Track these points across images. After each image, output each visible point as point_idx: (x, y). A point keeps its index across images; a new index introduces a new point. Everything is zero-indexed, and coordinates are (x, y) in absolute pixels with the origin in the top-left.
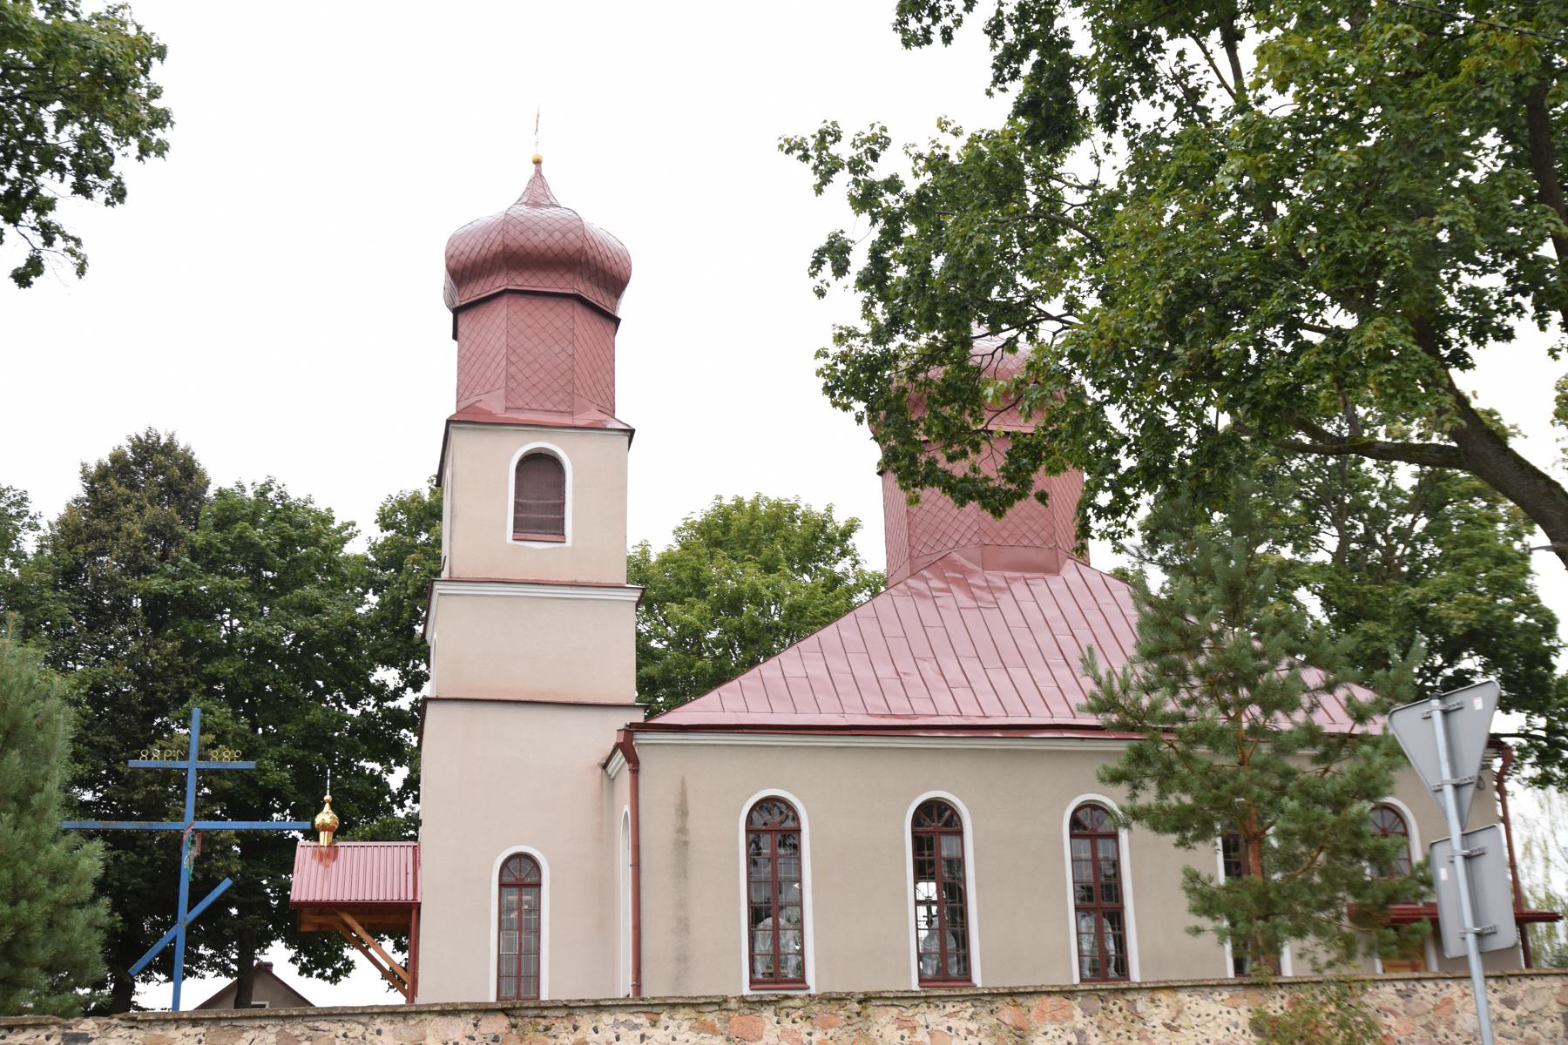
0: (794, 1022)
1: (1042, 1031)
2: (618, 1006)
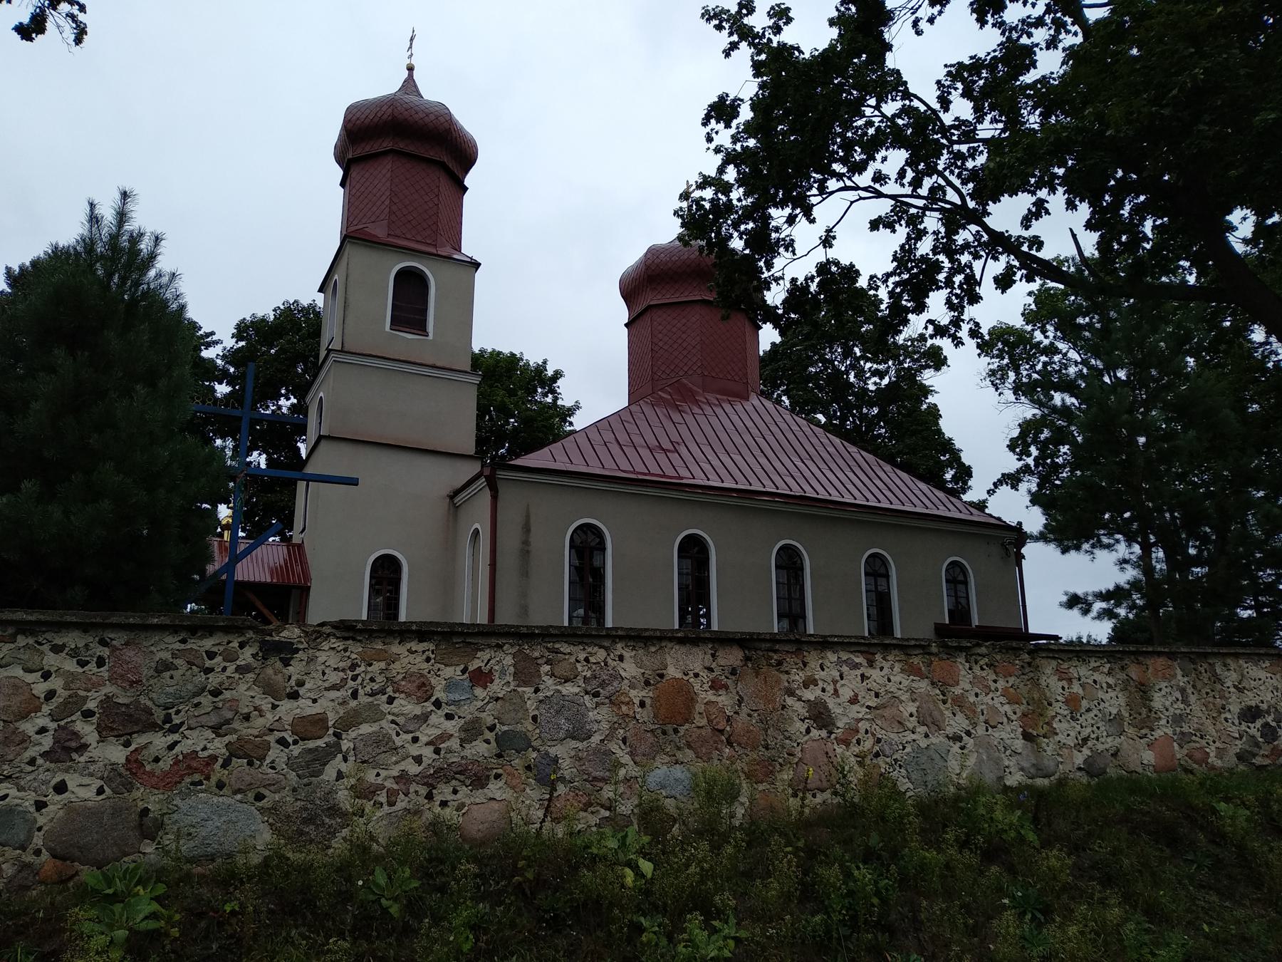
0: (982, 669)
1: (1157, 687)
2: (842, 643)
